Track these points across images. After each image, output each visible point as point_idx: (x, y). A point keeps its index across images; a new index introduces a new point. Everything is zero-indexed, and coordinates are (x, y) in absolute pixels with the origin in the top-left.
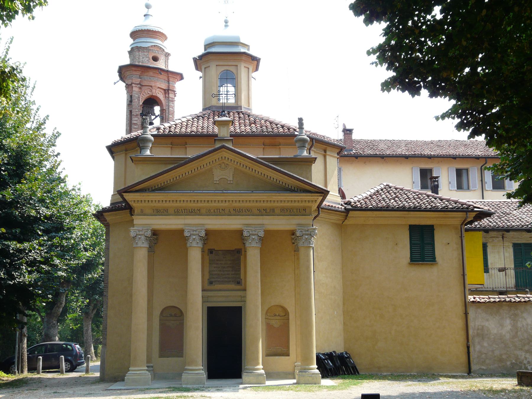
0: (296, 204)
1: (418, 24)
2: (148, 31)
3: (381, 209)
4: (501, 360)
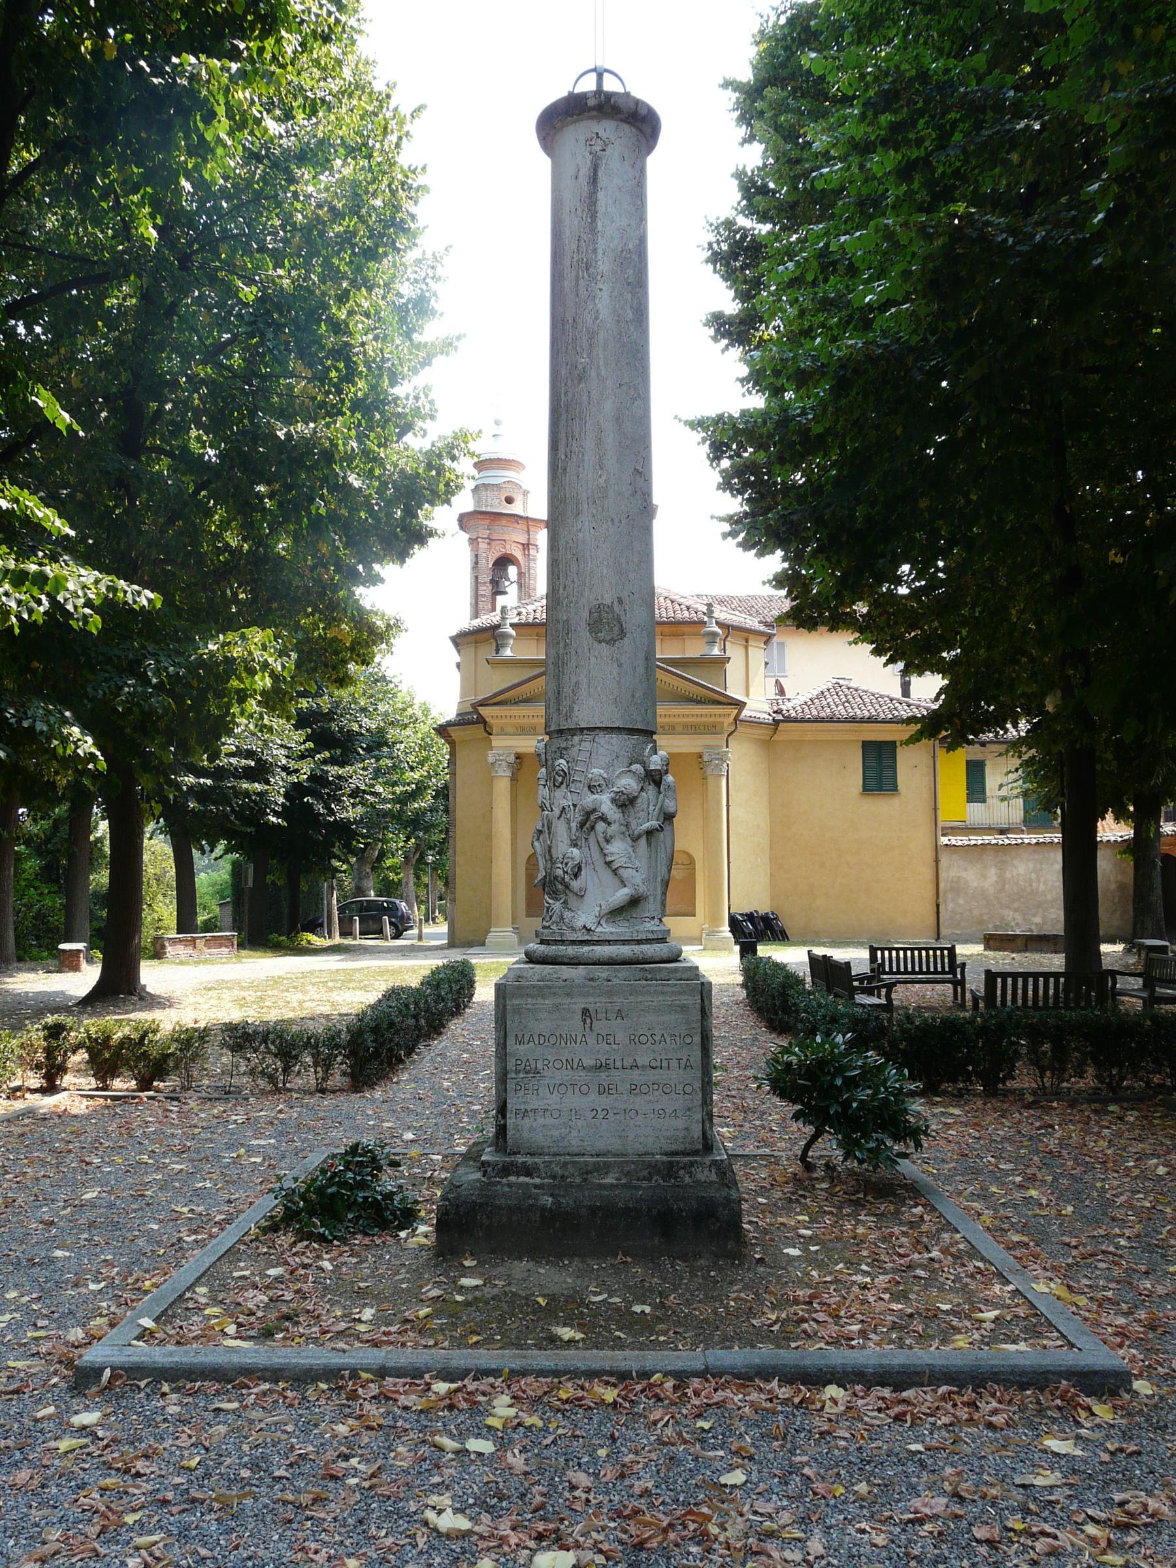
0: (704, 719)
2: (499, 460)
3: (822, 720)
4: (981, 922)
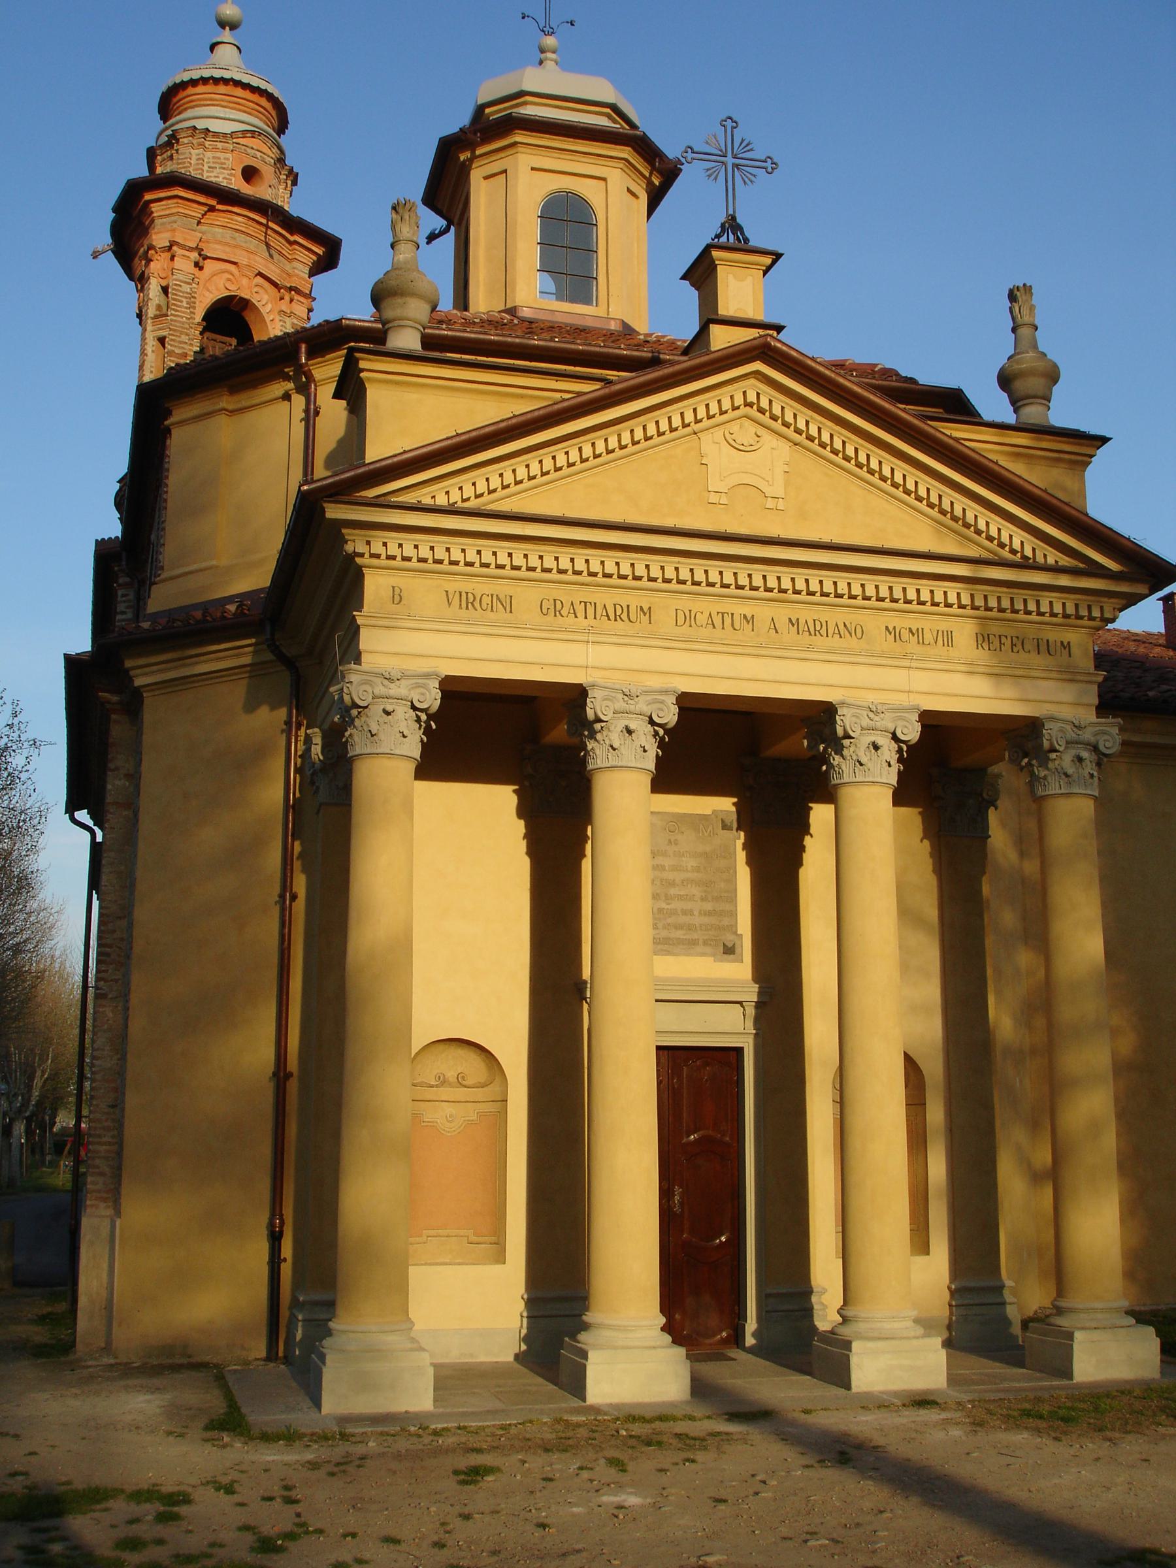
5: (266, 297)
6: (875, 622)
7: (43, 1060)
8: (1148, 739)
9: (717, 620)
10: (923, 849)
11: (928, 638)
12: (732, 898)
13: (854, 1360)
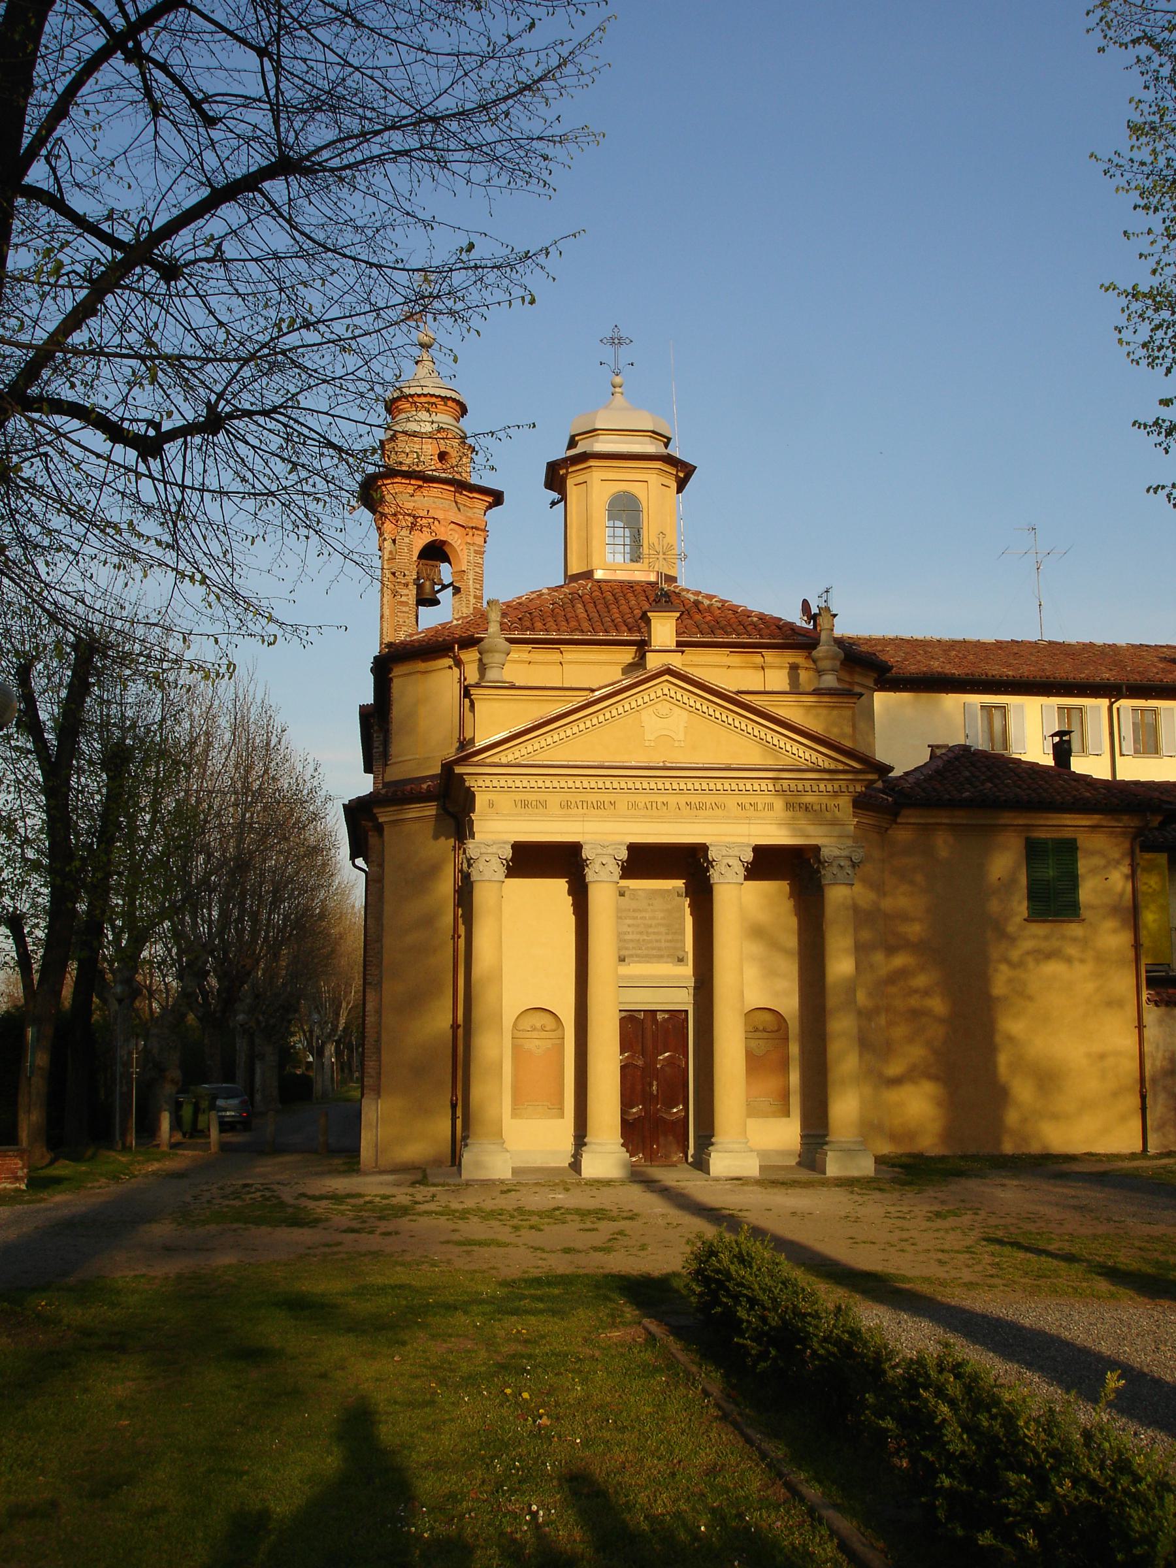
1: (92, 675)
5: (457, 536)
6: (731, 801)
7: (347, 993)
8: (958, 821)
9: (649, 806)
10: (789, 905)
11: (760, 807)
12: (683, 932)
13: (711, 1161)
